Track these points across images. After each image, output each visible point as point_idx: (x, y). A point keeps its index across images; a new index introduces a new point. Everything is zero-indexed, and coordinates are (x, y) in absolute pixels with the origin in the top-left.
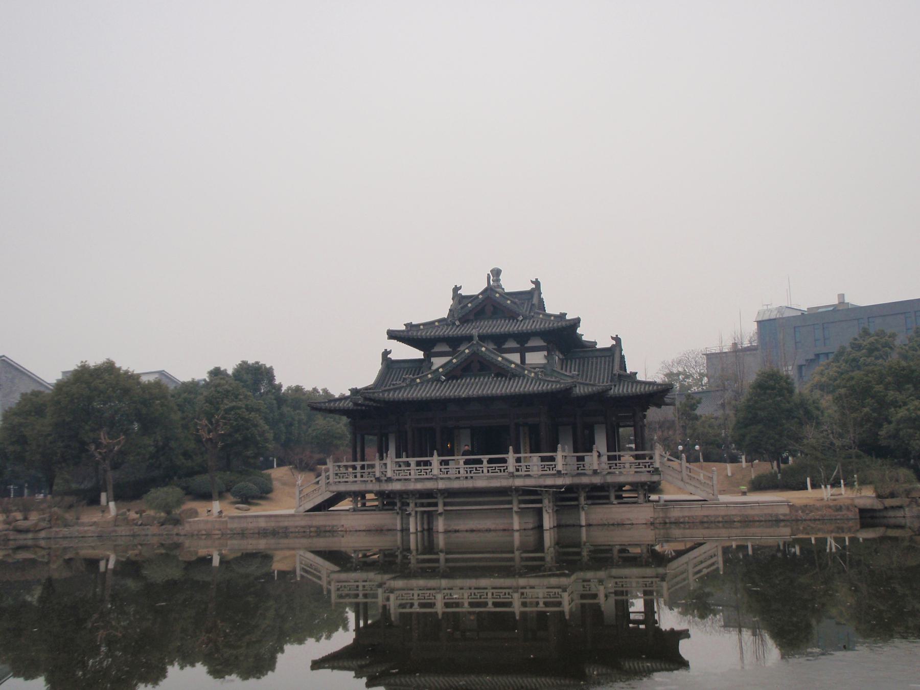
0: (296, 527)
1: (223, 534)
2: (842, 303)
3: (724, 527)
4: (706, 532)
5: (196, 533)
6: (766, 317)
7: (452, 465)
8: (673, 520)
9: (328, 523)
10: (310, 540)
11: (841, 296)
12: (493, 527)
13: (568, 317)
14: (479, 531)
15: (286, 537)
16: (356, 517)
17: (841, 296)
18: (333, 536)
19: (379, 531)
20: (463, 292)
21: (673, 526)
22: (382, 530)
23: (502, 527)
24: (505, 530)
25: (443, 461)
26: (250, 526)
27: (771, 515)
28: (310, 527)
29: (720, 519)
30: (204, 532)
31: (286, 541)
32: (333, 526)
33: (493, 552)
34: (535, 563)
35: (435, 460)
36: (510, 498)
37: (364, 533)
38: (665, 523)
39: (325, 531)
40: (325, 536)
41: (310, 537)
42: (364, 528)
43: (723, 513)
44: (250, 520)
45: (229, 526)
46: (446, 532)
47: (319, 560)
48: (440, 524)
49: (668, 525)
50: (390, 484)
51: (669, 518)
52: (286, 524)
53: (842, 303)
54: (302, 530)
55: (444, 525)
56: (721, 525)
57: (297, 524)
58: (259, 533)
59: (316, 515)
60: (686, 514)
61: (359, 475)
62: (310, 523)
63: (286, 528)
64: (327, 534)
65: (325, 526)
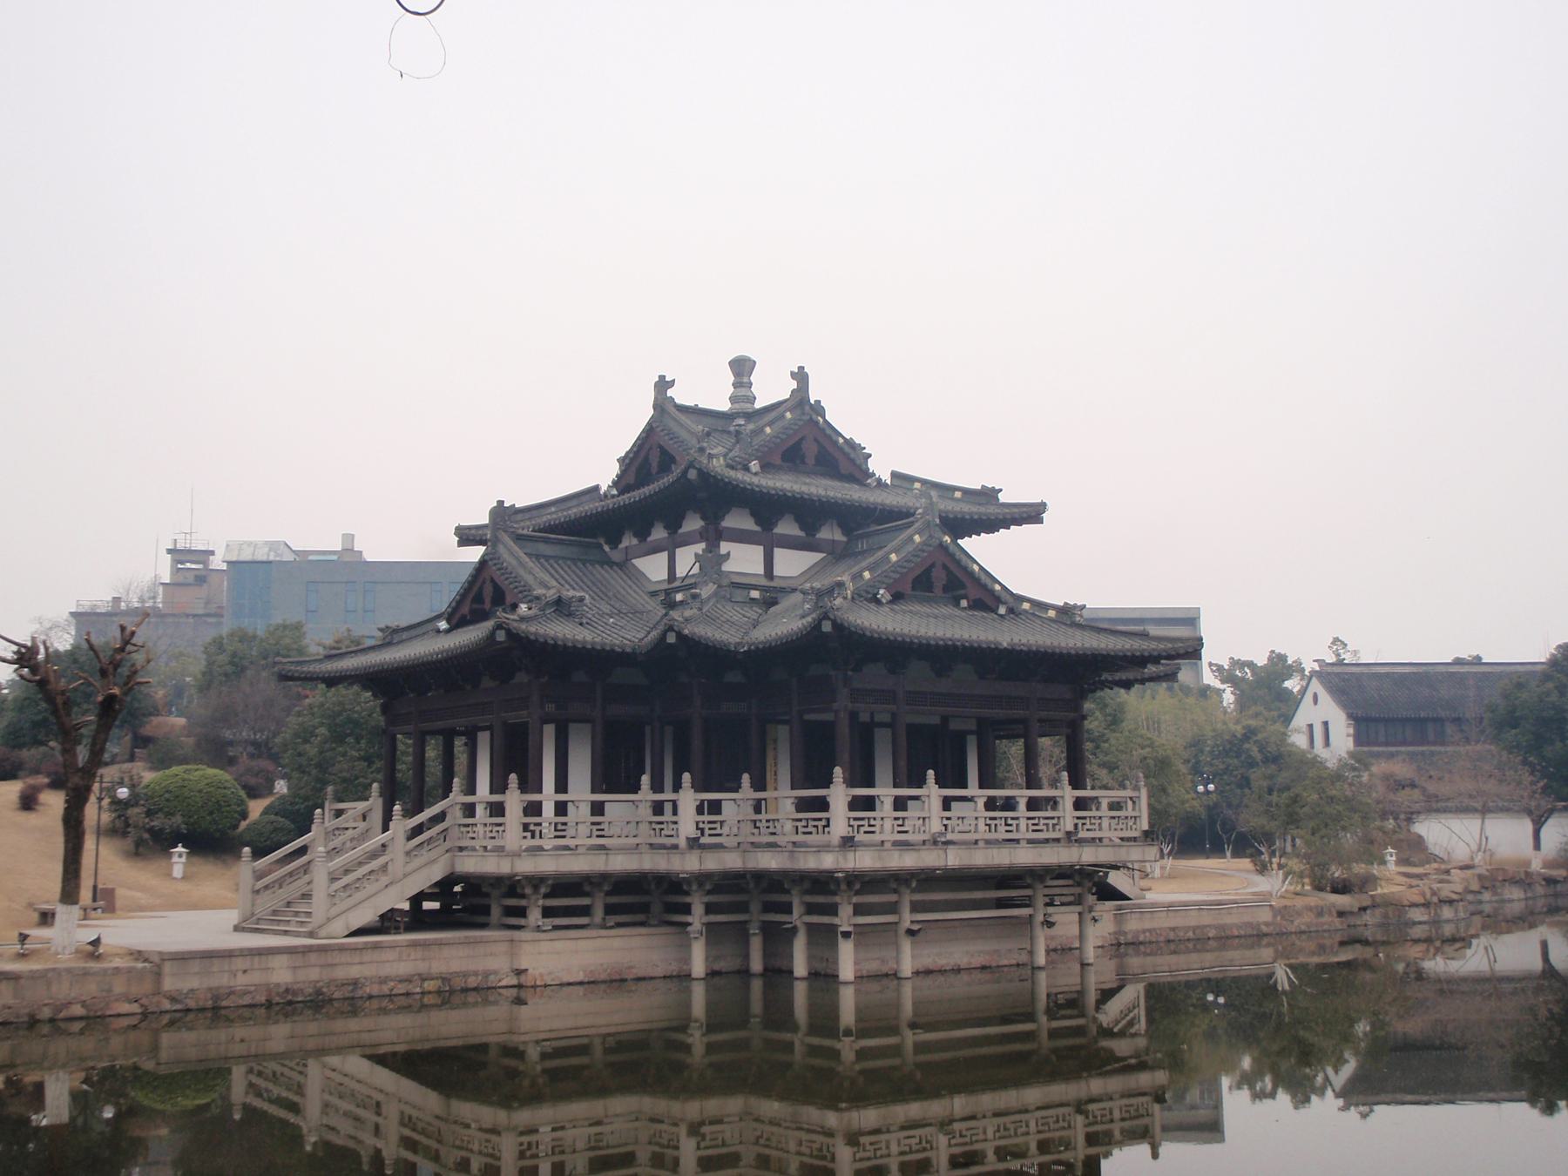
0: (383, 980)
1: (145, 1015)
2: (348, 551)
3: (1196, 950)
4: (353, 969)
5: (46, 1013)
6: (246, 556)
7: (913, 811)
8: (1130, 938)
9: (470, 966)
10: (421, 1018)
11: (349, 538)
12: (964, 961)
13: (1002, 498)
14: (942, 972)
15: (354, 1012)
16: (559, 945)
17: (349, 538)
18: (486, 1002)
19: (617, 983)
20: (681, 395)
21: (1130, 950)
22: (623, 980)
23: (978, 961)
24: (983, 968)
25: (855, 798)
26: (241, 981)
27: (1250, 924)
28: (423, 978)
29: (1190, 934)
30: (78, 1010)
31: (353, 1024)
32: (487, 974)
33: (1005, 1020)
34: (1018, 1047)
35: (932, 792)
36: (585, 901)
37: (580, 990)
38: (1119, 944)
39: (465, 990)
40: (465, 1005)
41: (424, 1007)
42: (581, 977)
43: (1193, 923)
44: (240, 963)
45: (168, 984)
46: (859, 978)
47: (385, 1078)
48: (847, 961)
49: (1122, 949)
50: (850, 855)
51: (1125, 933)
52: (354, 972)
53: (348, 551)
54: (402, 989)
55: (811, 958)
56: (1191, 945)
57: (387, 970)
58: (269, 1005)
59: (376, 947)
60: (1147, 925)
61: (547, 830)
62: (422, 967)
63: (355, 983)
64: (471, 998)
65: (465, 975)
